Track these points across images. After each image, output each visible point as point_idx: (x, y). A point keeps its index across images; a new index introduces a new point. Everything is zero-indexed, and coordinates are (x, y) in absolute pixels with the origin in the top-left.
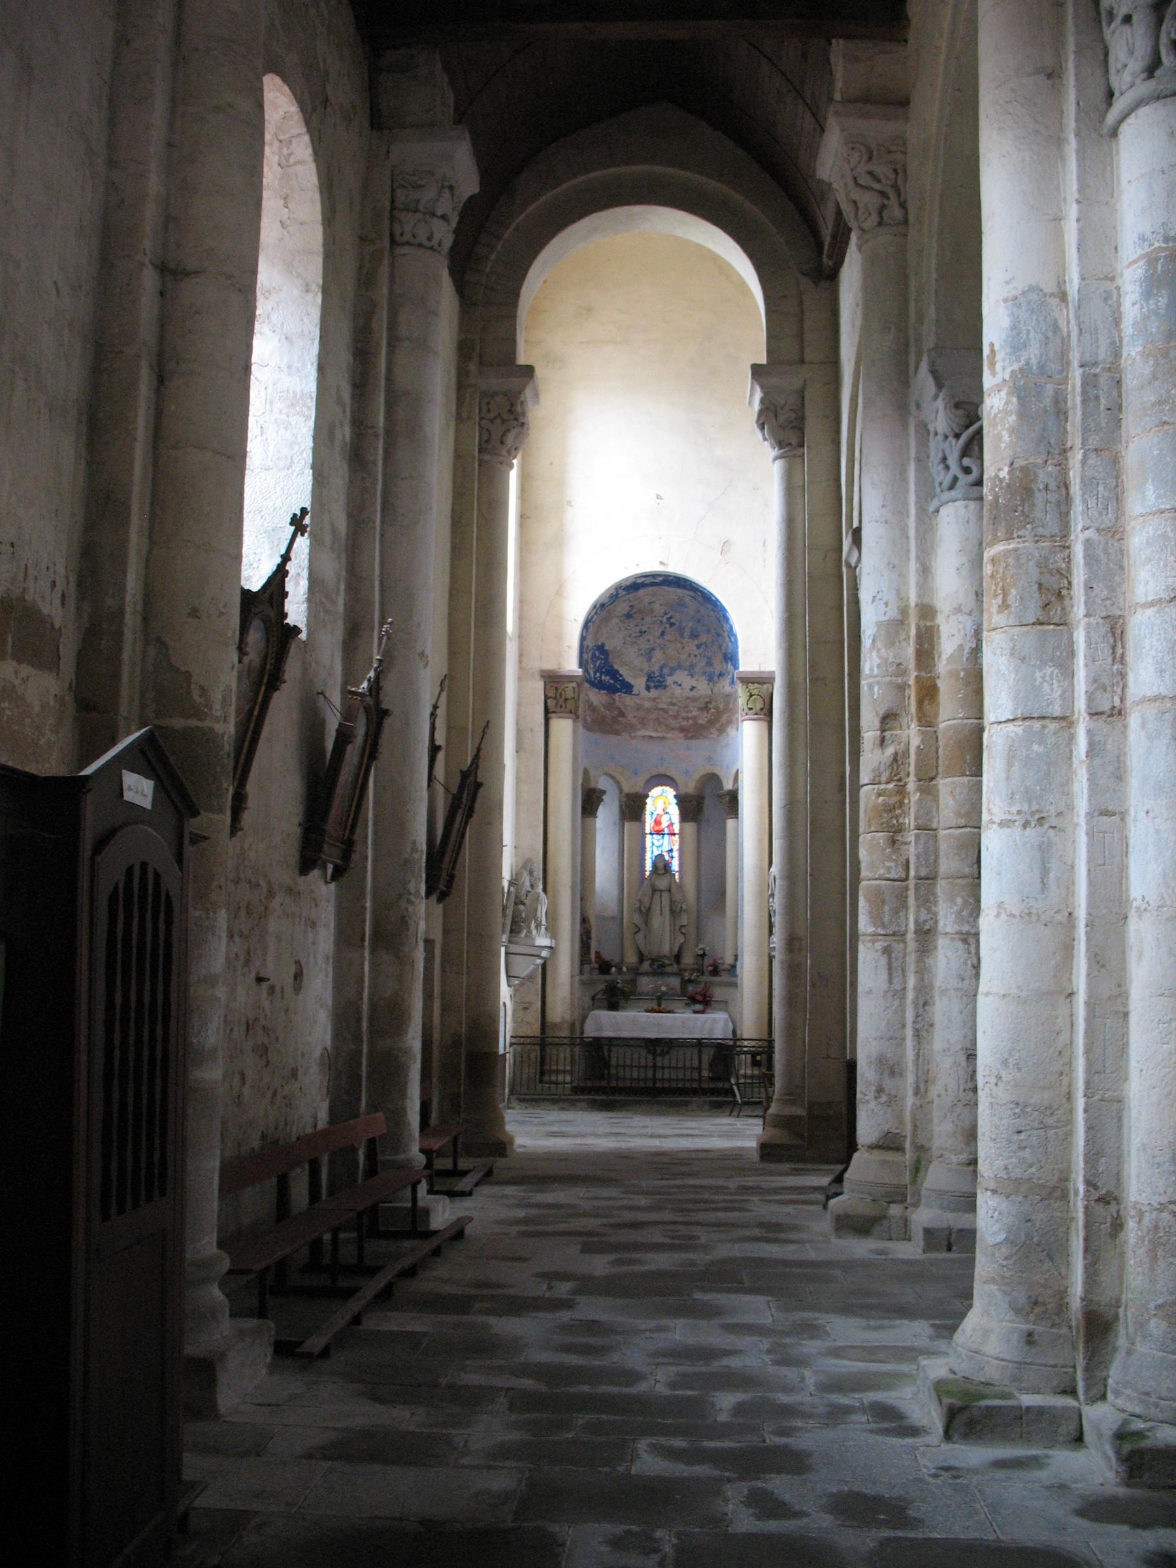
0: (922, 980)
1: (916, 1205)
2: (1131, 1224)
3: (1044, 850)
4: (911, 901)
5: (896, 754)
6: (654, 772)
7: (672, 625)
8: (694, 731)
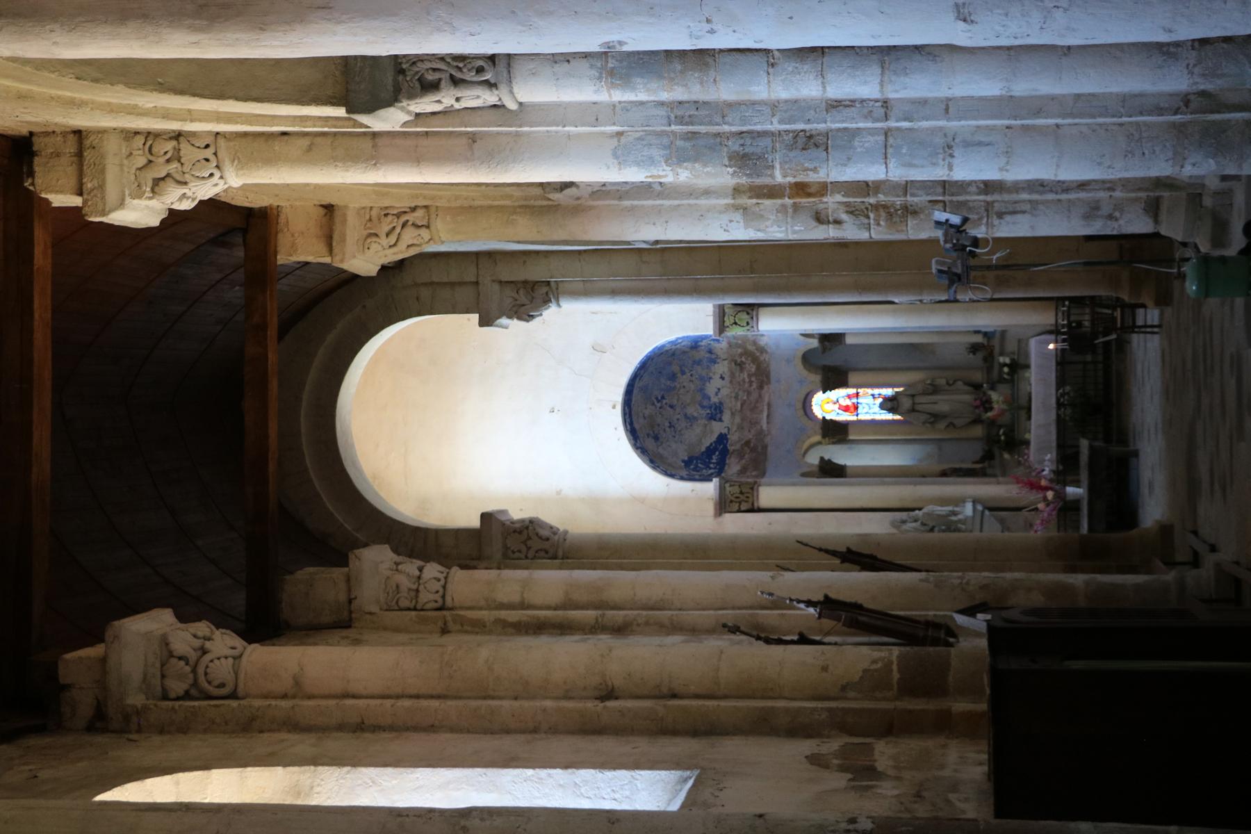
0: (1023, 189)
1: (1203, 186)
2: (1202, 87)
3: (967, 144)
4: (961, 198)
5: (847, 212)
6: (802, 412)
7: (663, 398)
8: (762, 375)
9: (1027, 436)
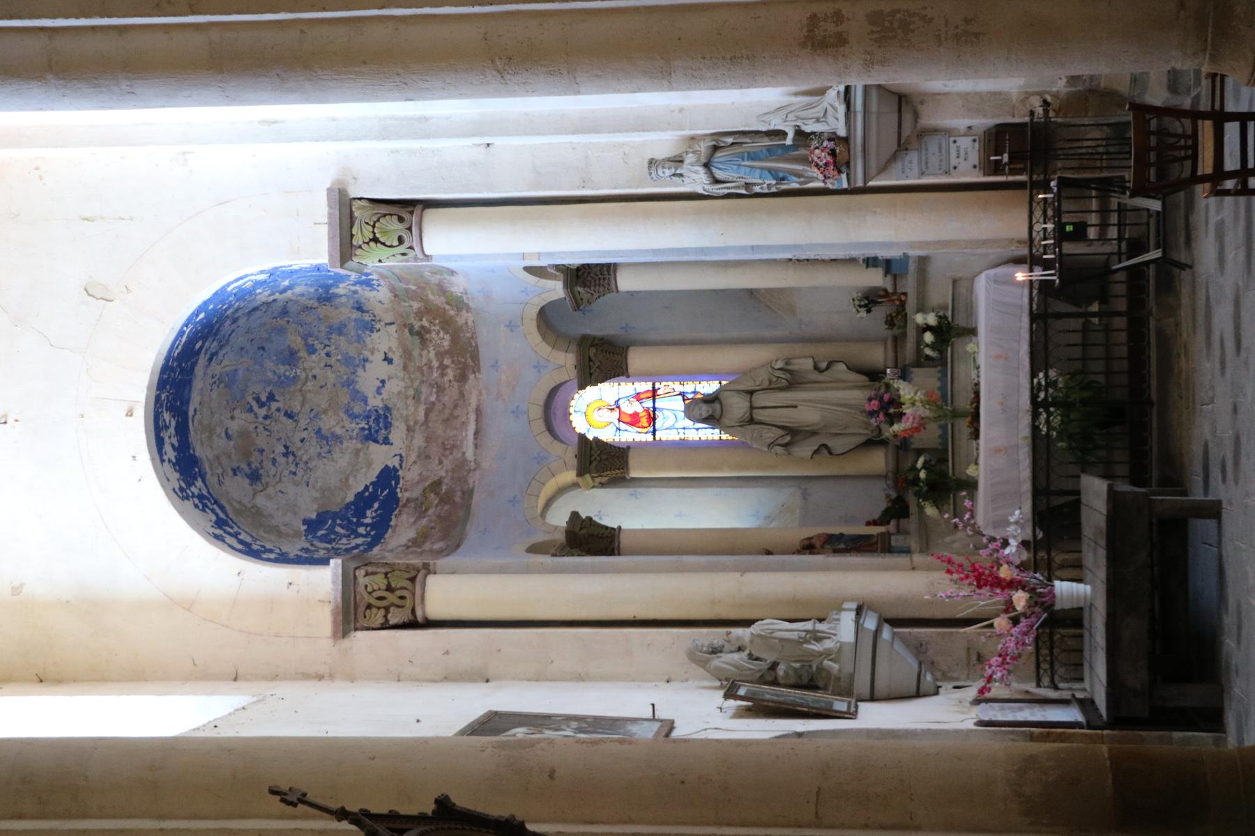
6: (540, 426)
7: (271, 397)
8: (465, 355)
9: (971, 471)
